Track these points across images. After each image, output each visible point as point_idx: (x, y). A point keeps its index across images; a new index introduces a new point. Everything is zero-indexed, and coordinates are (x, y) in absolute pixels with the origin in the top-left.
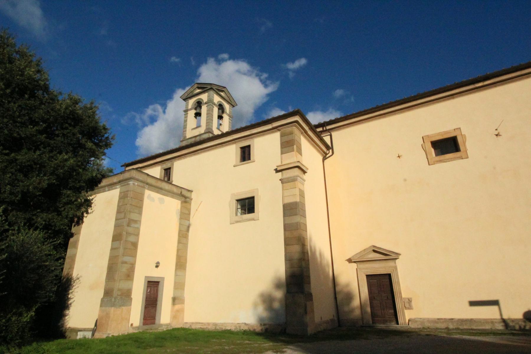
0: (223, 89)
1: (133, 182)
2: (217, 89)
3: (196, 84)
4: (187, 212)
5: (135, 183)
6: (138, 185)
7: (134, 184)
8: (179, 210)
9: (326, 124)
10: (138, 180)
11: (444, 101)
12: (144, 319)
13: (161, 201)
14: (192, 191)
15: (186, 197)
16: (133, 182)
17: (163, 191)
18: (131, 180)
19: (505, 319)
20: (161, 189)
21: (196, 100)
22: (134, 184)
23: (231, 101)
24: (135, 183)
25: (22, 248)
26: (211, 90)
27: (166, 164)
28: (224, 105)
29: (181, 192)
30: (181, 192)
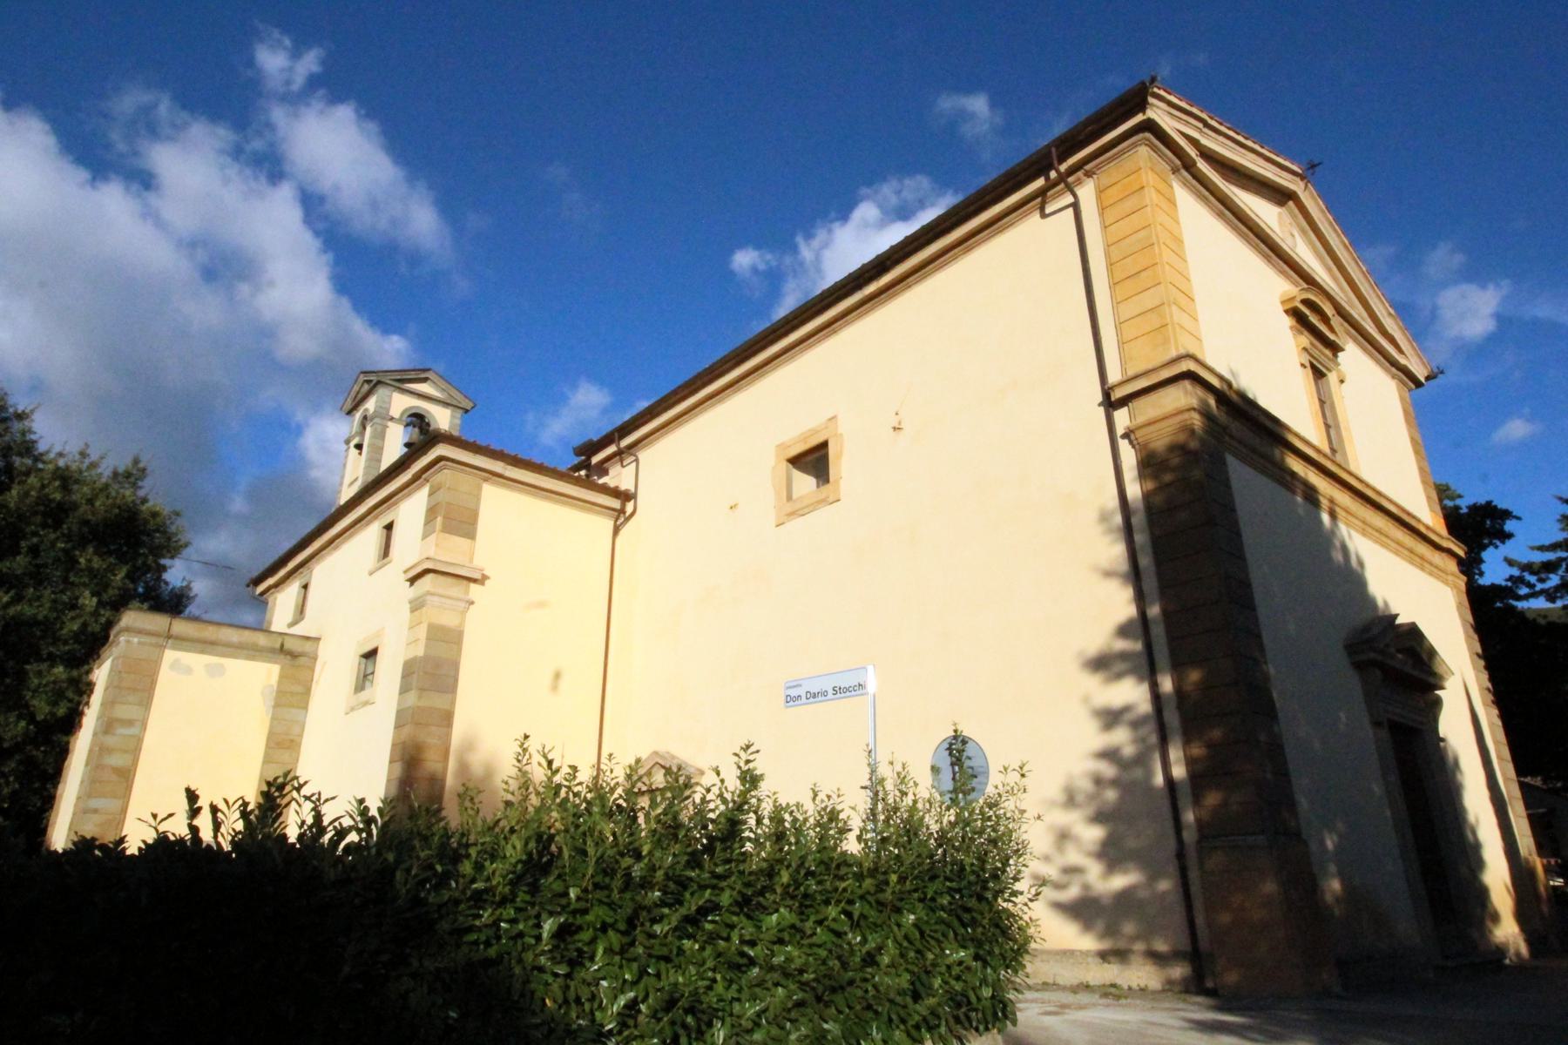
0: (423, 376)
1: (127, 638)
2: (391, 380)
3: (362, 375)
4: (299, 689)
5: (131, 639)
6: (139, 643)
7: (128, 642)
8: (272, 686)
9: (616, 435)
10: (140, 632)
11: (860, 316)
12: (986, 775)
13: (214, 672)
14: (318, 639)
15: (293, 655)
16: (127, 638)
17: (220, 648)
18: (122, 634)
19: (1491, 903)
20: (213, 643)
21: (418, 407)
22: (128, 642)
23: (460, 402)
24: (131, 639)
25: (1470, 533)
26: (379, 386)
27: (305, 574)
28: (428, 412)
29: (282, 645)
30: (282, 645)
